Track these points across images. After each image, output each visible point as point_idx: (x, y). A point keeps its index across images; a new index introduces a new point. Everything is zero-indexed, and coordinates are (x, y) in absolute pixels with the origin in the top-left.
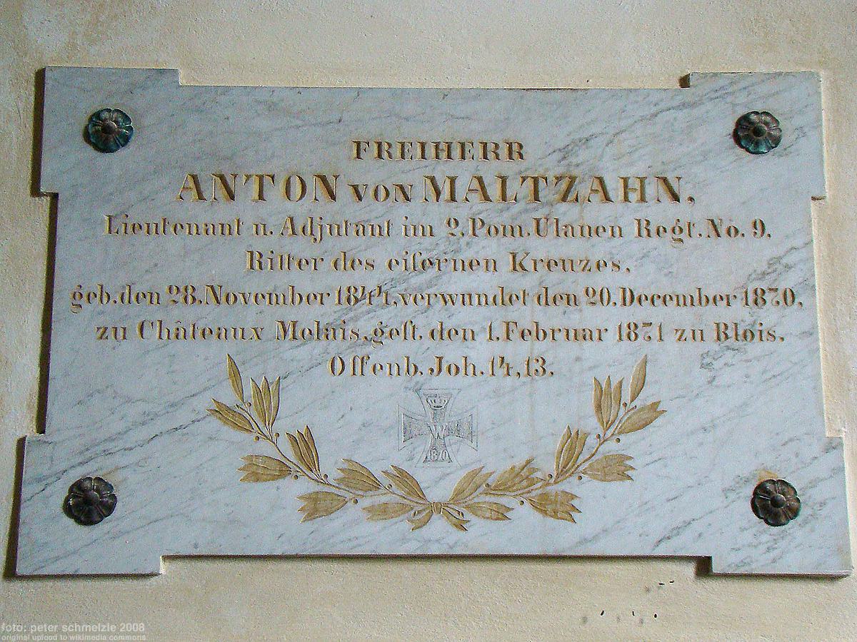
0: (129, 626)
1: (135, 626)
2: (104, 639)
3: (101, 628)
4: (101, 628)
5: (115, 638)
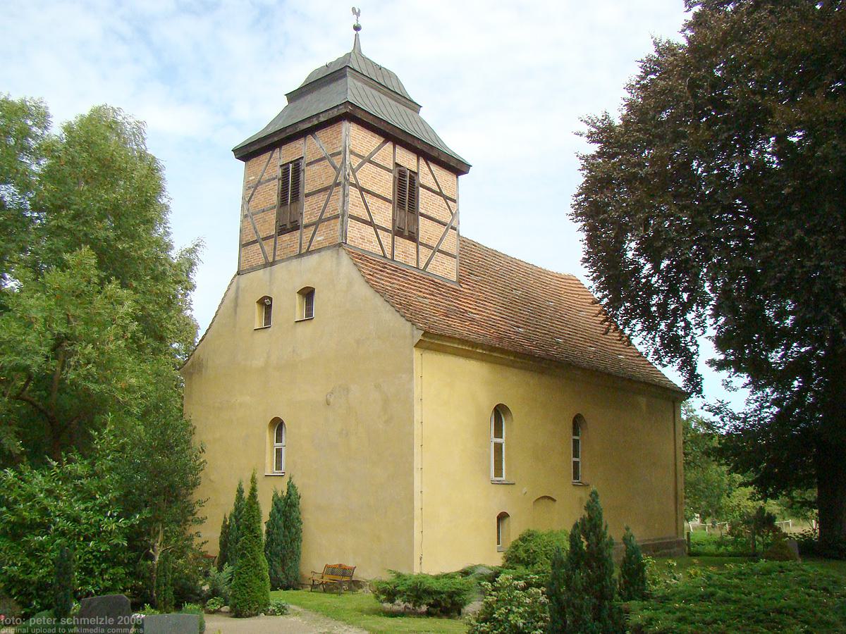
0: (127, 619)
1: (127, 619)
2: (103, 631)
3: (99, 621)
4: (99, 621)
5: (114, 631)
